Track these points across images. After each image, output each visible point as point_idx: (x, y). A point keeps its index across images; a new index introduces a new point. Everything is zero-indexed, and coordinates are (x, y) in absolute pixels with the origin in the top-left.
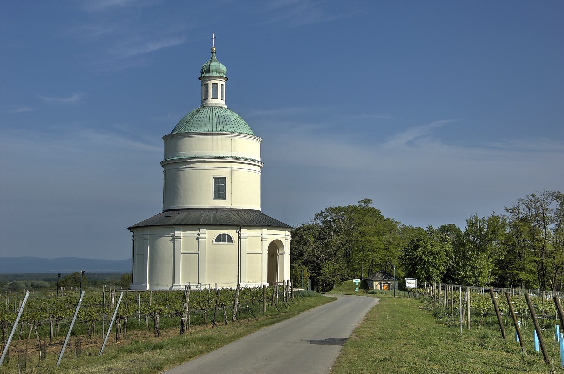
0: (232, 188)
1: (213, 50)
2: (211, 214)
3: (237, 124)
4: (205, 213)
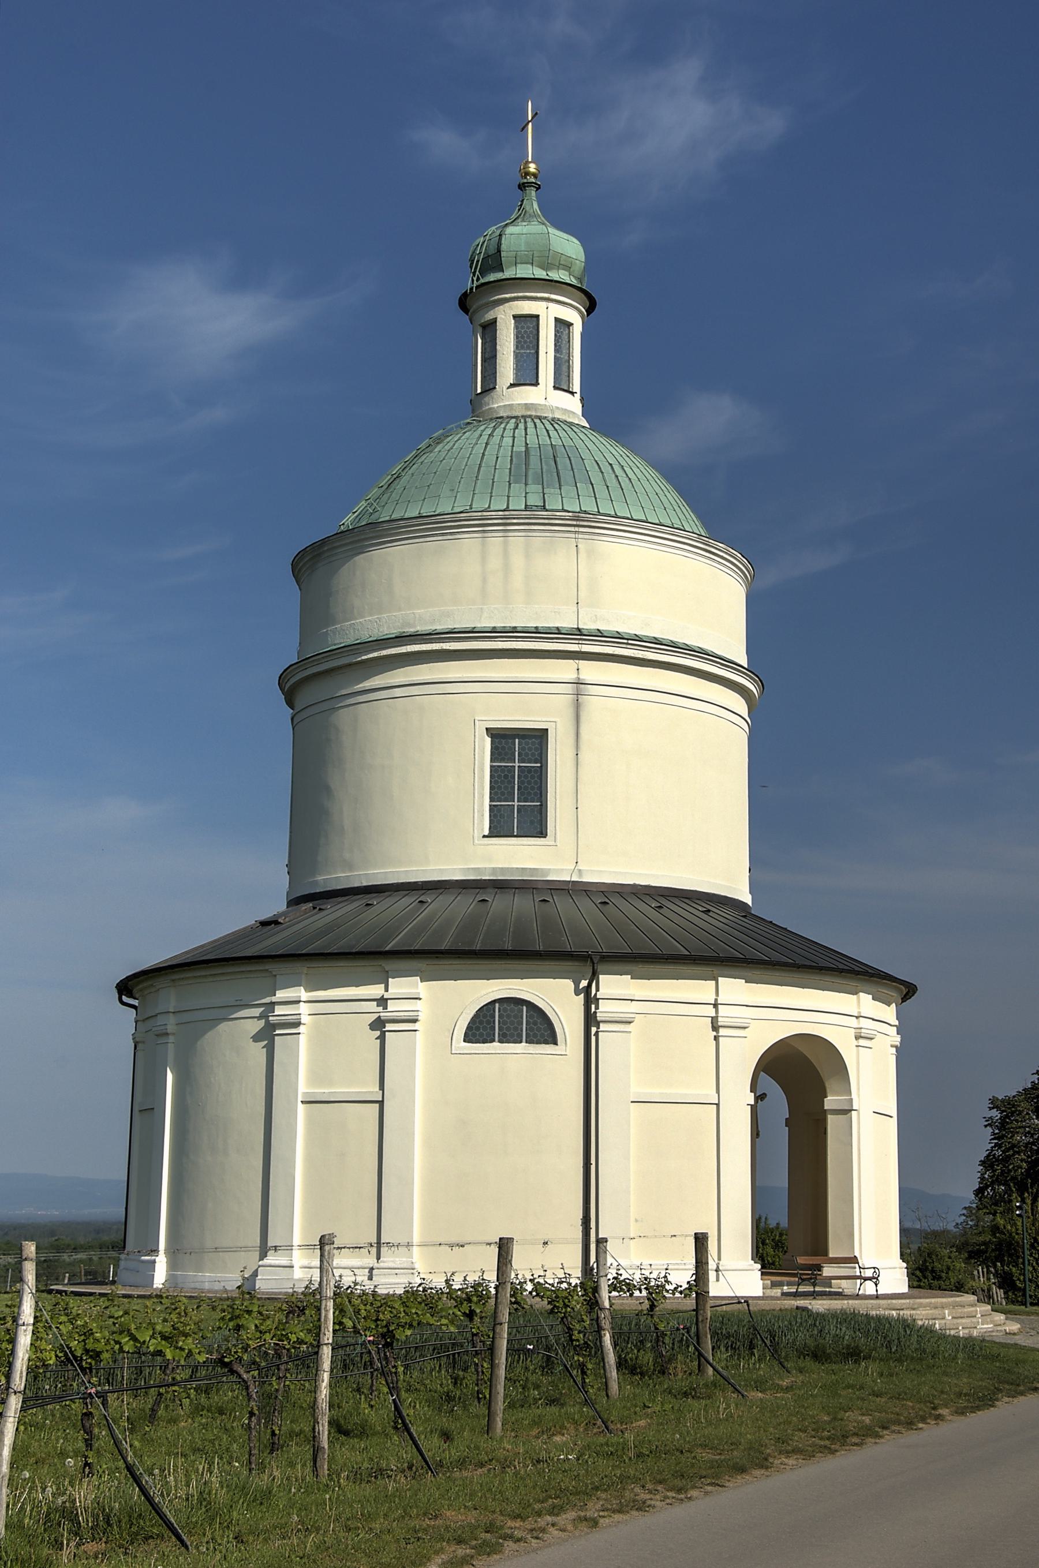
0: (577, 779)
1: (527, 174)
2: (464, 905)
3: (612, 483)
4: (437, 904)
